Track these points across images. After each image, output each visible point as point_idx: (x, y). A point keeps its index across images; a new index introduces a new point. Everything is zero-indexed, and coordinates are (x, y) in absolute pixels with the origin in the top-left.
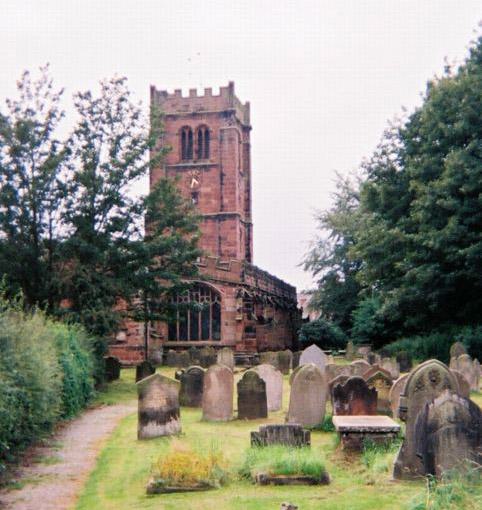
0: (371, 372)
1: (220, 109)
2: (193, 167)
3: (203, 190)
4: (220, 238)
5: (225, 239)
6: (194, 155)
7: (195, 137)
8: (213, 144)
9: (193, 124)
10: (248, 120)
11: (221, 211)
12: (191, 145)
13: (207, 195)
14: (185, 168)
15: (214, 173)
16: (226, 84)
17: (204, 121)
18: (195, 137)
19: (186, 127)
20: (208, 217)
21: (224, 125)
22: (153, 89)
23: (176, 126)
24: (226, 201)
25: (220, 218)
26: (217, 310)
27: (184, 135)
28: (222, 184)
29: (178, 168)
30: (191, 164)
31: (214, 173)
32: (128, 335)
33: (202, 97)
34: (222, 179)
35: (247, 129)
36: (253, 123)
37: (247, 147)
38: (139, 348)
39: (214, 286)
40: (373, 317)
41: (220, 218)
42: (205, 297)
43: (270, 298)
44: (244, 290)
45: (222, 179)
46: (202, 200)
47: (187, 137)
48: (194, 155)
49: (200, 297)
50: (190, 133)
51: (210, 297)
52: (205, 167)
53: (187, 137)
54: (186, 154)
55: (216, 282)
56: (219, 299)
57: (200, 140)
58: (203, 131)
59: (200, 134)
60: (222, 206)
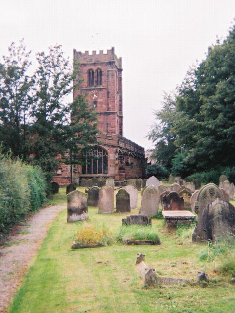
4: (107, 124)
5: (110, 124)
7: (95, 75)
8: (104, 78)
9: (94, 68)
10: (121, 66)
11: (108, 110)
13: (101, 103)
14: (90, 90)
15: (105, 92)
17: (99, 67)
18: (95, 75)
19: (99, 69)
20: (101, 114)
21: (109, 68)
22: (74, 51)
24: (110, 106)
25: (107, 114)
27: (89, 73)
28: (108, 97)
29: (87, 89)
30: (93, 87)
31: (105, 92)
32: (62, 171)
34: (108, 95)
35: (120, 70)
36: (123, 67)
38: (68, 178)
39: (104, 147)
41: (107, 114)
43: (131, 153)
44: (119, 149)
45: (108, 95)
46: (99, 105)
47: (91, 74)
50: (93, 72)
52: (100, 89)
53: (91, 74)
54: (91, 83)
55: (105, 145)
57: (97, 76)
58: (99, 71)
59: (98, 73)
60: (108, 108)
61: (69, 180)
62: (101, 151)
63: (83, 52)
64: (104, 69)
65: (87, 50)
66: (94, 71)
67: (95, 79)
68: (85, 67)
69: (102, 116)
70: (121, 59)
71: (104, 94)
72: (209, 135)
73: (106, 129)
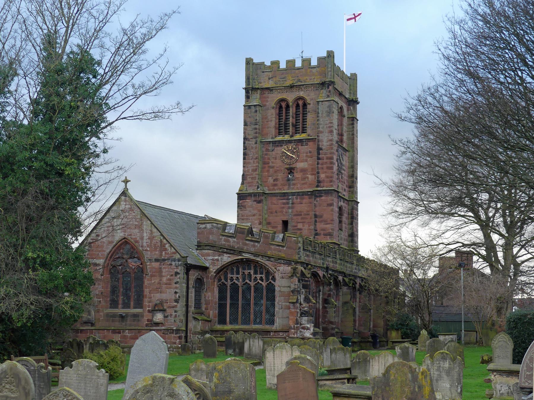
0: (322, 362)
1: (317, 81)
2: (289, 142)
3: (300, 165)
4: (316, 216)
5: (321, 217)
6: (291, 129)
7: (292, 111)
8: (310, 117)
9: (291, 97)
10: (355, 92)
11: (317, 186)
12: (287, 119)
13: (303, 171)
14: (280, 143)
15: (311, 147)
16: (325, 54)
17: (302, 94)
18: (292, 111)
19: (301, 98)
20: (304, 194)
21: (323, 95)
22: (249, 62)
23: (274, 98)
24: (322, 176)
25: (315, 194)
26: (271, 289)
27: (281, 107)
28: (319, 159)
29: (274, 143)
30: (287, 137)
31: (311, 147)
32: (165, 317)
33: (298, 69)
34: (319, 154)
35: (353, 102)
36: (360, 96)
37: (353, 120)
38: (178, 331)
39: (267, 263)
40: (310, 304)
41: (315, 194)
42: (258, 276)
43: (347, 280)
44: (300, 268)
45: (319, 154)
46: (298, 175)
47: (284, 110)
48: (291, 129)
49: (253, 277)
50: (288, 106)
51: (263, 276)
52: (300, 141)
53: (284, 110)
54: (282, 129)
55: (269, 258)
56: (274, 279)
57: (297, 115)
58: (301, 103)
59: (298, 106)
60: (319, 182)
61: (180, 338)
62: (261, 273)
63: (268, 63)
64: (309, 96)
65: (275, 59)
66: (291, 104)
67: (291, 120)
68: (270, 95)
69: (306, 200)
70: (354, 78)
71: (310, 152)
72: (17, 55)
73: (312, 227)
